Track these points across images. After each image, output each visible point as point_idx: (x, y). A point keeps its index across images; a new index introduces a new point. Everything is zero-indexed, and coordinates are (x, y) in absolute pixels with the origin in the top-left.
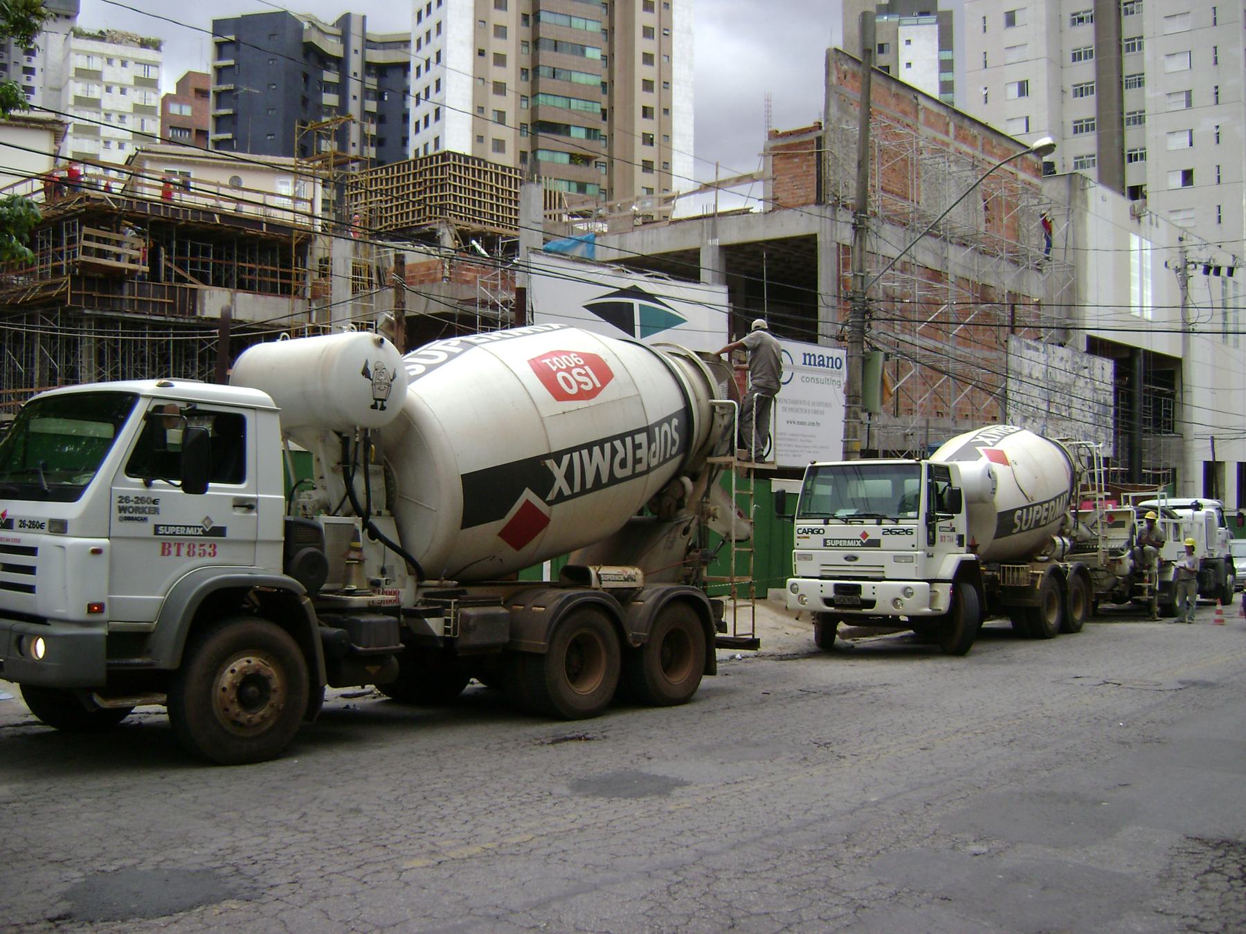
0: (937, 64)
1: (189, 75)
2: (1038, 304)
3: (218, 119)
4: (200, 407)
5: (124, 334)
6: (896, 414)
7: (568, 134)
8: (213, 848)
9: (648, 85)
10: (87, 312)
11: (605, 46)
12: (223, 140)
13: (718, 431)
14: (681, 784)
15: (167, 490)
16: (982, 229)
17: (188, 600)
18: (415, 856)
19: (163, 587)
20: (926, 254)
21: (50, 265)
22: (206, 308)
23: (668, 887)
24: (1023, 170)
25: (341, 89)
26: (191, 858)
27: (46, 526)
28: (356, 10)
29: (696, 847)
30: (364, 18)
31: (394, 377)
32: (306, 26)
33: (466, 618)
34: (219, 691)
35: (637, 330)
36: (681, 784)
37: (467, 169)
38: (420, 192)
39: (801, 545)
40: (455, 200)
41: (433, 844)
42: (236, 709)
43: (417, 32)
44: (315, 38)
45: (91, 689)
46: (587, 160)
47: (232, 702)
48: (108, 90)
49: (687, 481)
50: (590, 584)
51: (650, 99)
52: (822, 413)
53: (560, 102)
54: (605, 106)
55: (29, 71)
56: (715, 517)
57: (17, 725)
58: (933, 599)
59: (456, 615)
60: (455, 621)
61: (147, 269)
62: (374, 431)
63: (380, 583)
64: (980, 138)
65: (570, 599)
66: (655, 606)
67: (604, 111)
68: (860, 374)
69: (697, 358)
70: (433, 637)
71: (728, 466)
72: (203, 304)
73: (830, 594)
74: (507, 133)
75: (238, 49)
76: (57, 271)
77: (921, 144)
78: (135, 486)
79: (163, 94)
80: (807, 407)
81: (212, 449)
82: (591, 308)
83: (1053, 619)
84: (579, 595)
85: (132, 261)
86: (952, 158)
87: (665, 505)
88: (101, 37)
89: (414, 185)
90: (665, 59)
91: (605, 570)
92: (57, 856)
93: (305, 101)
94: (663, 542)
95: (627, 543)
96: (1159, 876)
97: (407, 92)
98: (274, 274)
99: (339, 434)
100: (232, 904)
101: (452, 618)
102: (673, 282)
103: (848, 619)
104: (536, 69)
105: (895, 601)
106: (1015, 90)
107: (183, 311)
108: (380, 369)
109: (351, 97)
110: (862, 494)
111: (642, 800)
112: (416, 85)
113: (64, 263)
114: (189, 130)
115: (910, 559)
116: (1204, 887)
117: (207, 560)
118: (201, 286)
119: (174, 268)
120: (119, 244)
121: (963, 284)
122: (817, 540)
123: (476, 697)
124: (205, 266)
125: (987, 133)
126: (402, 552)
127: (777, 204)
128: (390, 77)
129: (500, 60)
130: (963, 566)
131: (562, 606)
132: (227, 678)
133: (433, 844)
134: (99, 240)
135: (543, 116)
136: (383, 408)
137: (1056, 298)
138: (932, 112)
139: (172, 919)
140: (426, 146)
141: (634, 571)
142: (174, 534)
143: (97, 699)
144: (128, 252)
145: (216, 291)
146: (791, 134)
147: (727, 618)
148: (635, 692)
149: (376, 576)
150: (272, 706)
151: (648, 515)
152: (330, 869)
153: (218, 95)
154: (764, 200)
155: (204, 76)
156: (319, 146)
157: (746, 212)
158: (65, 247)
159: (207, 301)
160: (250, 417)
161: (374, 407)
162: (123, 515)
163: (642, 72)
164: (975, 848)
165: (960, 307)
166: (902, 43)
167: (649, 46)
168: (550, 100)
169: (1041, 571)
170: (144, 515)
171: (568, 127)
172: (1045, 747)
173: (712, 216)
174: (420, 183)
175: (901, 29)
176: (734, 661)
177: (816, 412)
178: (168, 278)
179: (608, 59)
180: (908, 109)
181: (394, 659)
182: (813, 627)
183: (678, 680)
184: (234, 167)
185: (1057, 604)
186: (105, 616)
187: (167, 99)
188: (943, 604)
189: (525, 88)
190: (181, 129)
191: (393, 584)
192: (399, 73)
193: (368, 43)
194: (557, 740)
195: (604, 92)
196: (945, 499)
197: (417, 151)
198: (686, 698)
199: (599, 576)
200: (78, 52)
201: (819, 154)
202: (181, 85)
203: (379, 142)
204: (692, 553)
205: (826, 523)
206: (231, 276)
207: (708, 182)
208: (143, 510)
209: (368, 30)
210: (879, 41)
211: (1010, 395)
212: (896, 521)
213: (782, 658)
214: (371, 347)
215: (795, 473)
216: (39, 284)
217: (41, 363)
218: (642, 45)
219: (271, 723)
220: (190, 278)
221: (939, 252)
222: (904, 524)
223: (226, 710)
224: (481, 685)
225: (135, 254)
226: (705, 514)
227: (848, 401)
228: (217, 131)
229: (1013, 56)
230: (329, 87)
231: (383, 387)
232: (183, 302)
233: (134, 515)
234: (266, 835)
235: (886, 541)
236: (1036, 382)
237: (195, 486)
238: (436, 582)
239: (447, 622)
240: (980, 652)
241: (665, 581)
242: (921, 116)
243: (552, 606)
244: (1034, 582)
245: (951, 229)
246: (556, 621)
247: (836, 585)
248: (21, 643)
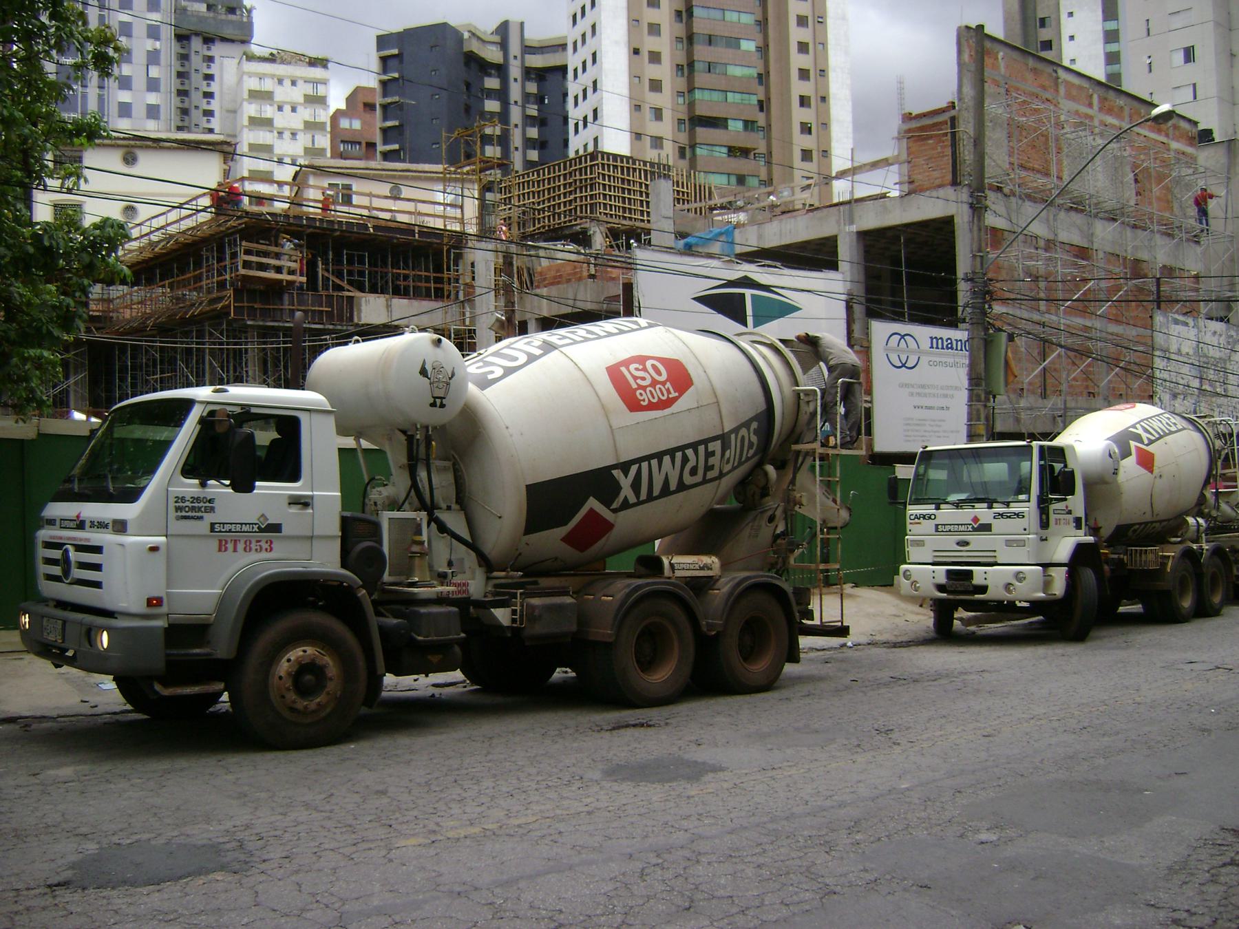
0: (1101, 35)
1: (357, 91)
2: (1197, 277)
3: (385, 131)
4: (254, 410)
5: (285, 342)
6: (1044, 396)
7: (726, 127)
8: (229, 825)
9: (804, 74)
10: (249, 323)
11: (760, 37)
12: (391, 151)
13: (804, 418)
14: (715, 769)
15: (219, 489)
16: (1132, 203)
17: (244, 591)
18: (413, 835)
19: (222, 580)
20: (1070, 230)
21: (215, 280)
22: (363, 315)
23: (643, 869)
24: (1175, 139)
25: (502, 95)
26: (201, 834)
27: (110, 526)
28: (514, 18)
29: (696, 831)
30: (522, 24)
31: (453, 375)
32: (466, 35)
33: (533, 607)
34: (277, 677)
35: (750, 320)
36: (715, 769)
37: (615, 167)
38: (570, 193)
39: (915, 531)
40: (605, 198)
41: (437, 824)
42: (292, 696)
43: (573, 35)
44: (475, 47)
45: (150, 678)
46: (745, 152)
47: (288, 689)
48: (280, 109)
49: (770, 469)
50: (662, 573)
51: (806, 88)
52: (952, 396)
53: (716, 96)
54: (762, 97)
55: (209, 95)
56: (801, 505)
57: (115, 713)
58: (1047, 584)
59: (522, 606)
60: (522, 611)
61: (304, 279)
62: (435, 428)
63: (446, 573)
64: (1127, 110)
65: (638, 587)
66: (731, 593)
67: (760, 103)
68: (982, 356)
69: (781, 346)
70: (499, 627)
71: (812, 453)
72: (360, 311)
73: (942, 580)
74: (665, 128)
75: (401, 62)
76: (222, 285)
77: (1063, 118)
78: (190, 486)
79: (332, 111)
80: (935, 391)
81: (270, 451)
82: (700, 299)
83: (1187, 603)
84: (648, 584)
85: (291, 272)
86: (1097, 131)
87: (750, 492)
88: (272, 59)
89: (565, 185)
91: (677, 560)
92: (84, 830)
93: (468, 109)
94: (747, 532)
95: (709, 532)
96: (1170, 868)
97: (565, 95)
98: (427, 279)
99: (404, 432)
100: (218, 876)
101: (518, 608)
102: (786, 271)
103: (969, 606)
104: (691, 64)
105: (1008, 586)
106: (1180, 56)
107: (341, 319)
108: (438, 368)
110: (975, 478)
111: (667, 785)
112: (573, 88)
113: (228, 277)
114: (360, 143)
115: (1021, 543)
116: (1214, 880)
117: (264, 555)
118: (357, 294)
119: (331, 277)
120: (277, 256)
121: (1112, 258)
122: (928, 526)
123: (564, 685)
124: (361, 274)
125: (1135, 104)
126: (472, 546)
127: (913, 189)
128: (549, 80)
129: (655, 57)
130: (1080, 549)
131: (628, 595)
132: (284, 667)
133: (437, 824)
134: (259, 254)
135: (700, 111)
136: (442, 406)
137: (1215, 269)
138: (1073, 85)
139: (158, 887)
140: (585, 146)
141: (712, 561)
142: (230, 531)
143: (158, 687)
144: (287, 263)
145: (372, 298)
146: (924, 115)
147: (814, 605)
148: (711, 679)
149: (443, 569)
150: (328, 693)
151: (733, 504)
152: (327, 846)
153: (385, 107)
154: (900, 183)
155: (372, 90)
156: (483, 152)
157: (883, 196)
158: (228, 262)
159: (363, 307)
160: (304, 419)
161: (433, 405)
162: (179, 514)
163: (798, 61)
164: (984, 836)
165: (1112, 282)
166: (1064, 16)
167: (803, 34)
168: (706, 95)
169: (1171, 553)
170: (199, 514)
171: (726, 119)
172: (1118, 733)
173: (849, 202)
174: (570, 184)
176: (844, 649)
177: (946, 396)
178: (326, 287)
179: (763, 50)
180: (1047, 83)
181: (457, 649)
182: (932, 614)
183: (759, 667)
185: (1191, 587)
186: (164, 609)
187: (338, 115)
188: (1059, 587)
189: (682, 84)
190: (353, 143)
191: (460, 576)
192: (559, 76)
193: (528, 49)
194: (618, 727)
195: (761, 83)
196: (1058, 479)
197: (577, 152)
198: (768, 685)
199: (672, 565)
200: (250, 75)
201: (954, 134)
202: (350, 100)
203: (541, 145)
204: (779, 541)
205: (938, 508)
206: (387, 282)
207: (860, 171)
208: (199, 509)
209: (526, 36)
210: (1040, 15)
211: (1157, 373)
212: (1007, 504)
213: (895, 645)
214: (430, 348)
215: (907, 458)
216: (205, 298)
217: (211, 374)
219: (328, 710)
220: (347, 287)
221: (1085, 228)
222: (1015, 508)
223: (283, 697)
224: (574, 674)
225: (293, 265)
226: (791, 502)
227: (970, 384)
228: (385, 142)
229: (1178, 22)
230: (490, 94)
231: (441, 385)
232: (341, 310)
233: (190, 514)
234: (285, 814)
235: (998, 525)
236: (1185, 360)
237: (243, 485)
238: (503, 574)
239: (514, 612)
240: (1100, 638)
241: (752, 570)
242: (1062, 90)
243: (619, 596)
244: (1164, 565)
245: (1096, 204)
246: (642, 607)
247: (948, 572)
248: (90, 635)
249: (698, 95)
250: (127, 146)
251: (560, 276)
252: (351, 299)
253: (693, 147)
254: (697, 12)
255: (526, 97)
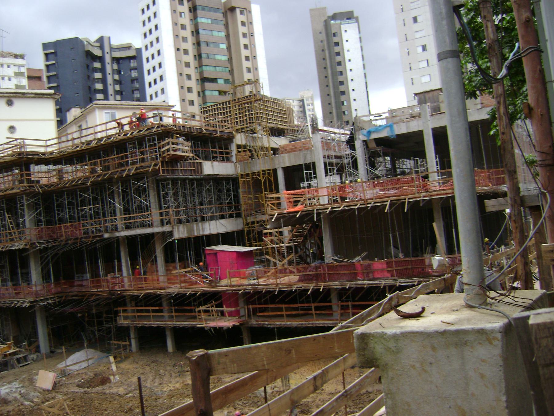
7: (217, 82)
10: (168, 177)
25: (102, 70)
28: (106, 35)
30: (109, 38)
32: (86, 43)
46: (225, 93)
53: (212, 69)
75: (56, 56)
90: (253, 46)
93: (89, 77)
109: (108, 74)
129: (186, 52)
135: (206, 75)
166: (343, 32)
168: (208, 68)
175: (342, 26)
179: (229, 48)
184: (133, 108)
193: (112, 49)
209: (112, 43)
210: (333, 32)
218: (243, 41)
225: (187, 148)
229: (418, 35)
249: (204, 68)
250: (8, 97)
251: (296, 148)
252: (201, 163)
253: (203, 91)
254: (201, 31)
255: (113, 70)
